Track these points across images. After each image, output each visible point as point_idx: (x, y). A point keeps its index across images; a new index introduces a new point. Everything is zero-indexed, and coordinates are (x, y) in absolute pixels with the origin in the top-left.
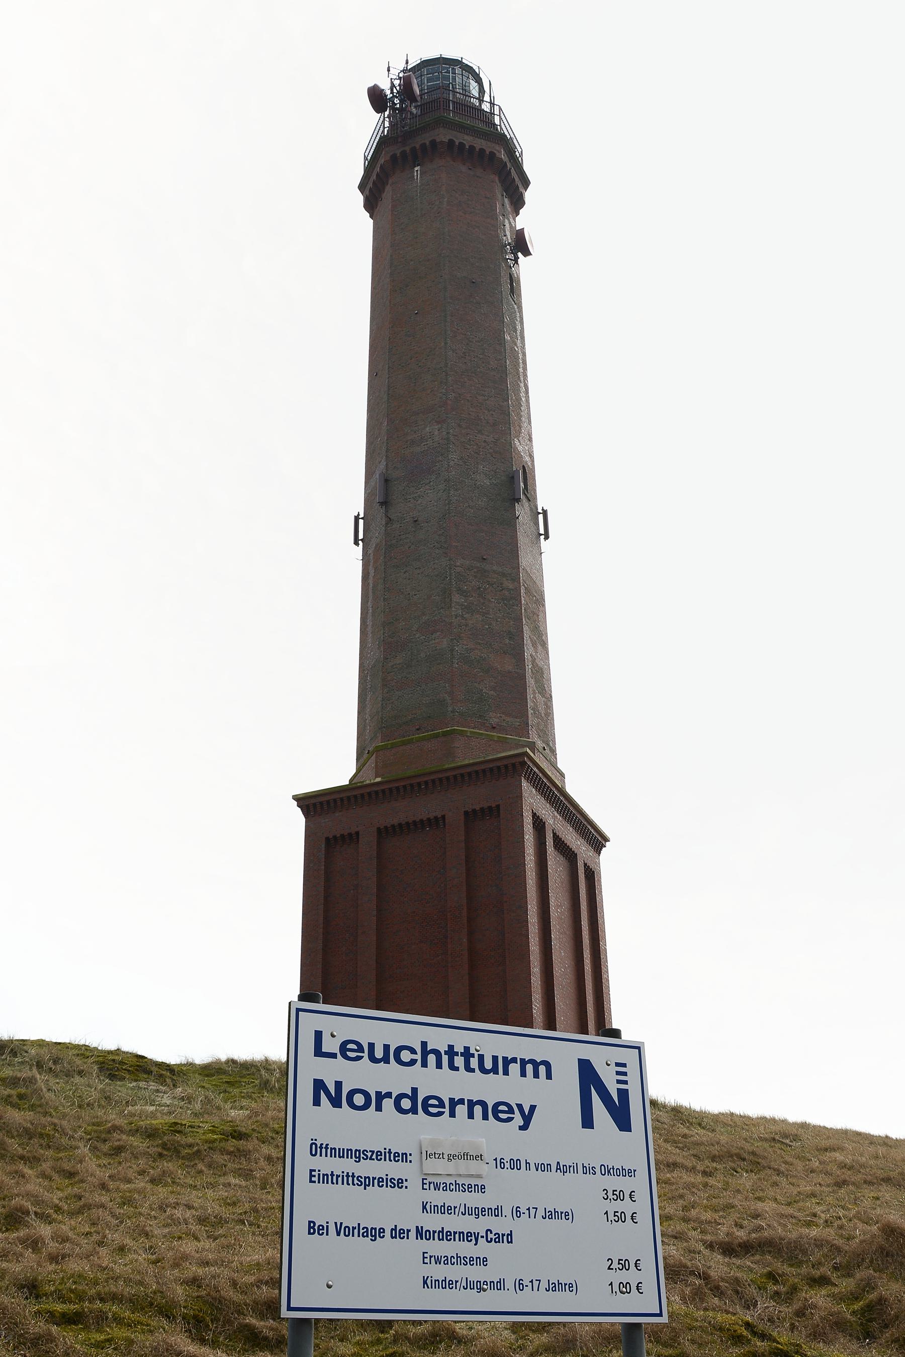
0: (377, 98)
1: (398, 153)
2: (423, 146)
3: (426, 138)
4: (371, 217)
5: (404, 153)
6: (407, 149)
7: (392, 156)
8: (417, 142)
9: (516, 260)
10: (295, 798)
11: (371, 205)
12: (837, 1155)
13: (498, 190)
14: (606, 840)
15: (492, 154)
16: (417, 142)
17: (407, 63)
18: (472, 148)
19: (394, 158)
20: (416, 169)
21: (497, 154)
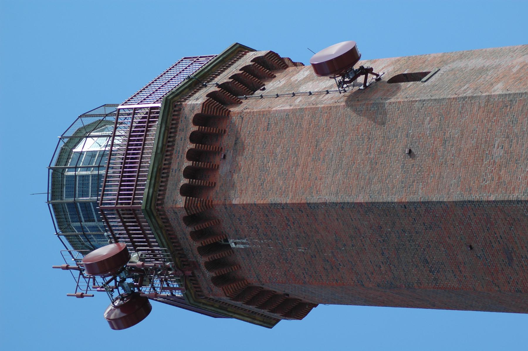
0: (133, 311)
1: (209, 275)
2: (196, 235)
3: (184, 231)
4: (316, 306)
5: (210, 266)
6: (202, 260)
7: (216, 284)
8: (192, 246)
9: (366, 71)
10: (314, 65)
11: (298, 309)
12: (300, 170)
13: (249, 106)
14: (74, 207)
15: (198, 120)
16: (192, 246)
17: (67, 268)
18: (191, 155)
19: (219, 281)
20: (233, 245)
21: (198, 111)
